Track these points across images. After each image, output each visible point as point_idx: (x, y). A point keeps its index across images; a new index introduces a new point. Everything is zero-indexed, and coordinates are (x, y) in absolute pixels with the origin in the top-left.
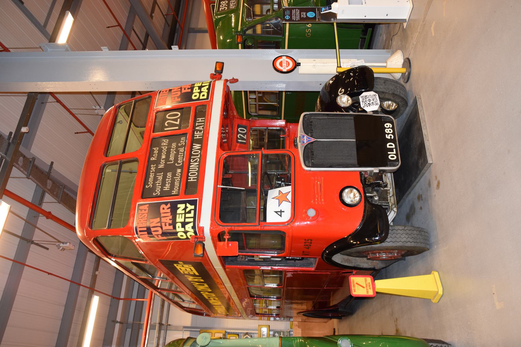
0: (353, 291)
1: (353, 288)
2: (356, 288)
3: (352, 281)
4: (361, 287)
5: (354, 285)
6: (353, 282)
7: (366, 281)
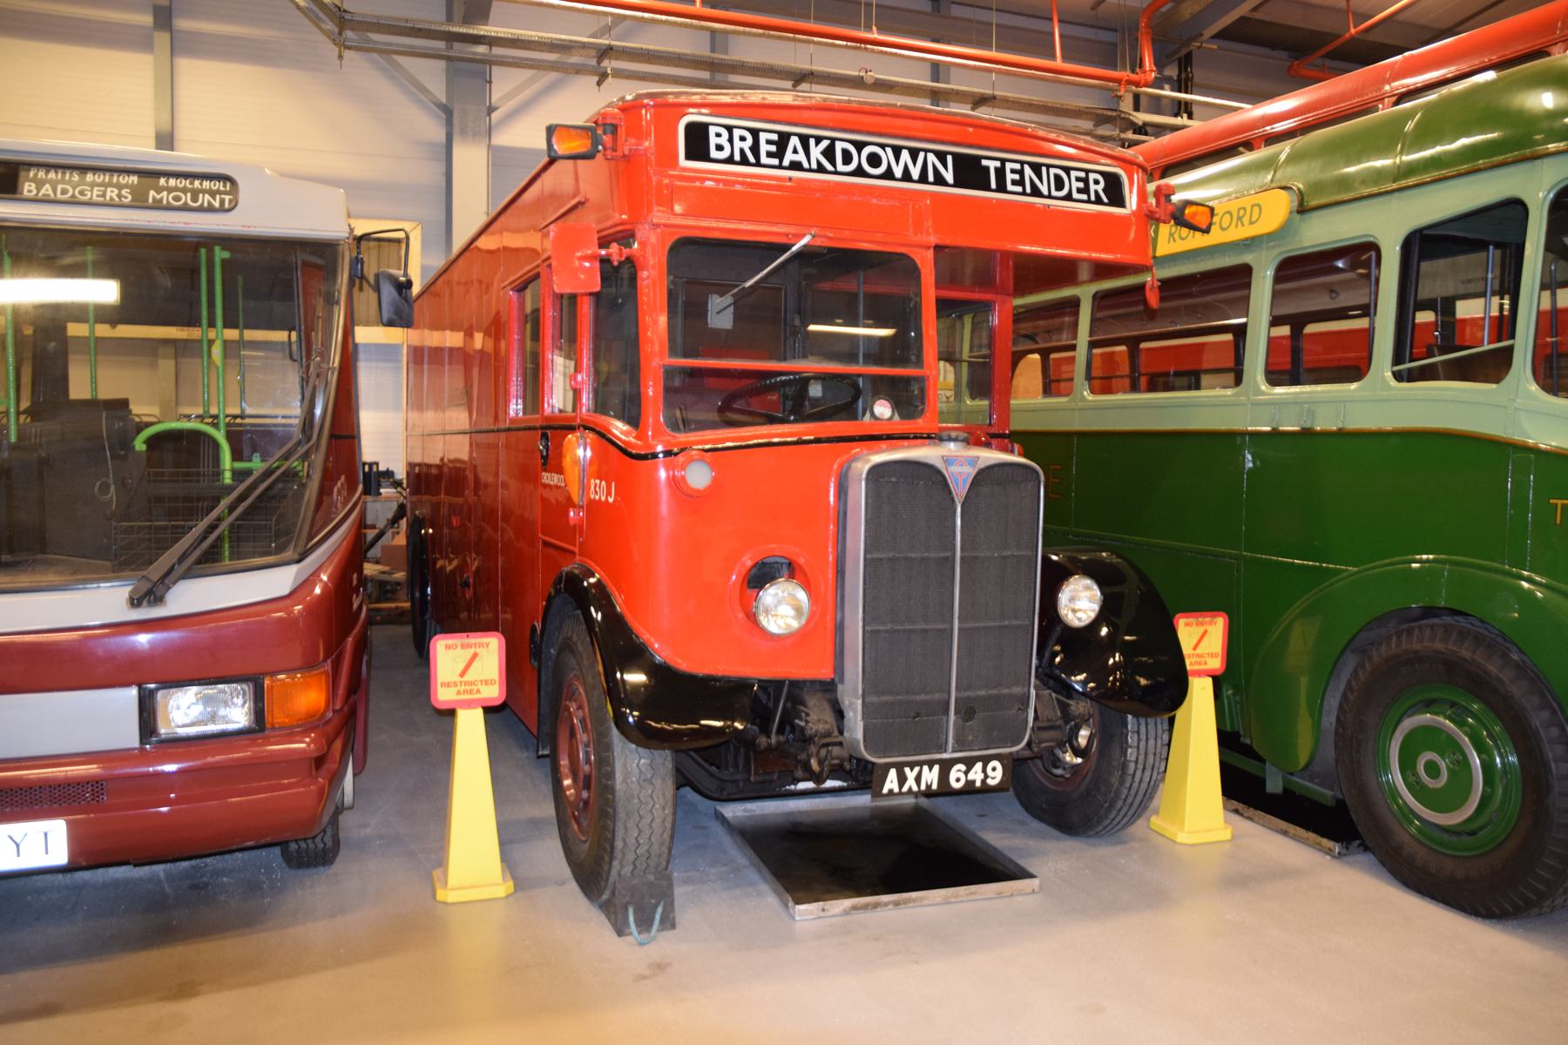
0: (450, 642)
1: (458, 642)
3: (486, 640)
5: (469, 646)
6: (481, 645)
7: (1212, 655)
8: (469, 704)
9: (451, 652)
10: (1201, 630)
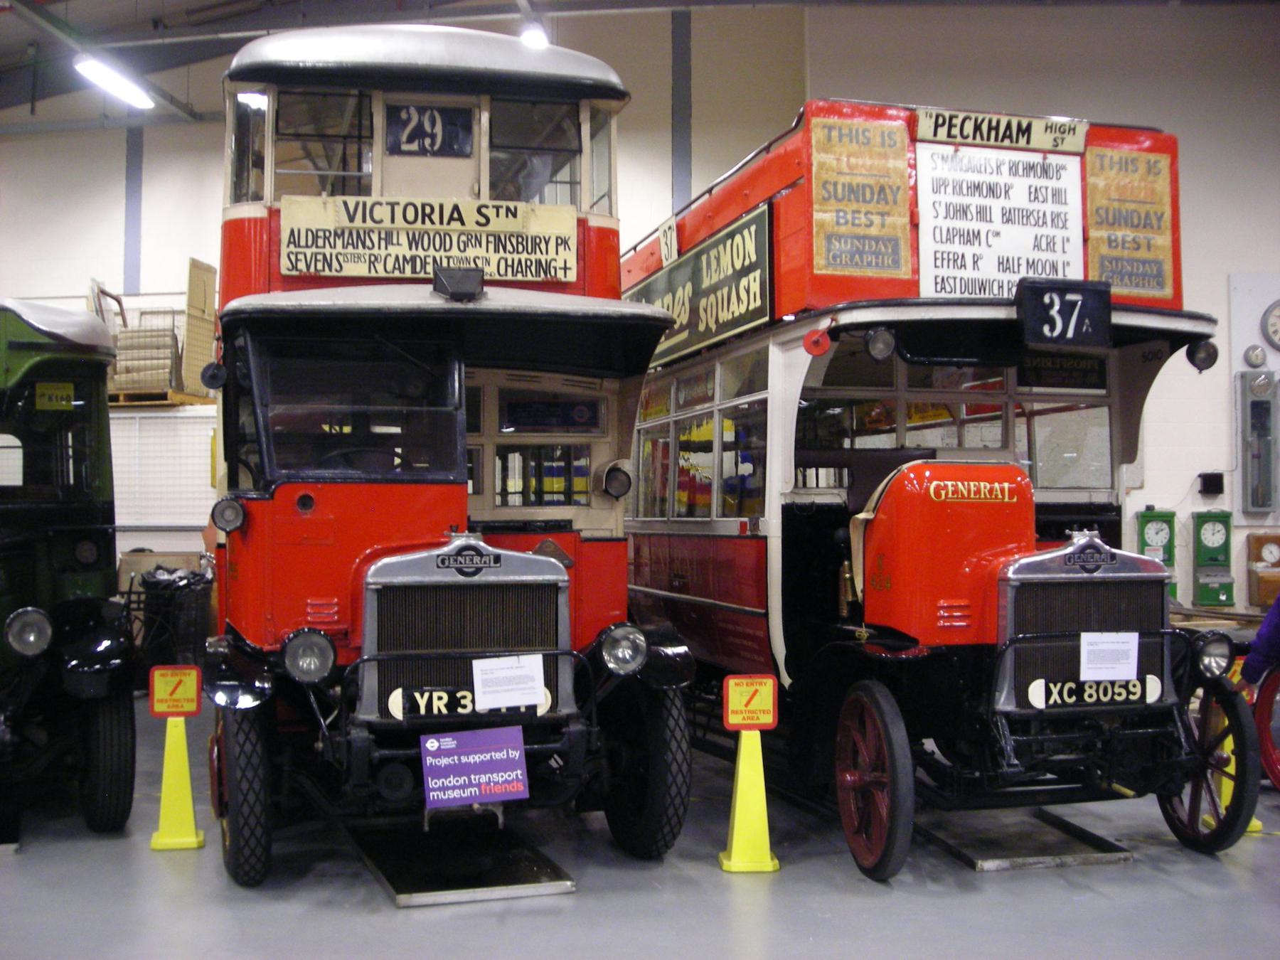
2: (744, 688)
4: (171, 689)
6: (761, 684)
7: (189, 700)
8: (750, 727)
9: (739, 689)
10: (177, 679)
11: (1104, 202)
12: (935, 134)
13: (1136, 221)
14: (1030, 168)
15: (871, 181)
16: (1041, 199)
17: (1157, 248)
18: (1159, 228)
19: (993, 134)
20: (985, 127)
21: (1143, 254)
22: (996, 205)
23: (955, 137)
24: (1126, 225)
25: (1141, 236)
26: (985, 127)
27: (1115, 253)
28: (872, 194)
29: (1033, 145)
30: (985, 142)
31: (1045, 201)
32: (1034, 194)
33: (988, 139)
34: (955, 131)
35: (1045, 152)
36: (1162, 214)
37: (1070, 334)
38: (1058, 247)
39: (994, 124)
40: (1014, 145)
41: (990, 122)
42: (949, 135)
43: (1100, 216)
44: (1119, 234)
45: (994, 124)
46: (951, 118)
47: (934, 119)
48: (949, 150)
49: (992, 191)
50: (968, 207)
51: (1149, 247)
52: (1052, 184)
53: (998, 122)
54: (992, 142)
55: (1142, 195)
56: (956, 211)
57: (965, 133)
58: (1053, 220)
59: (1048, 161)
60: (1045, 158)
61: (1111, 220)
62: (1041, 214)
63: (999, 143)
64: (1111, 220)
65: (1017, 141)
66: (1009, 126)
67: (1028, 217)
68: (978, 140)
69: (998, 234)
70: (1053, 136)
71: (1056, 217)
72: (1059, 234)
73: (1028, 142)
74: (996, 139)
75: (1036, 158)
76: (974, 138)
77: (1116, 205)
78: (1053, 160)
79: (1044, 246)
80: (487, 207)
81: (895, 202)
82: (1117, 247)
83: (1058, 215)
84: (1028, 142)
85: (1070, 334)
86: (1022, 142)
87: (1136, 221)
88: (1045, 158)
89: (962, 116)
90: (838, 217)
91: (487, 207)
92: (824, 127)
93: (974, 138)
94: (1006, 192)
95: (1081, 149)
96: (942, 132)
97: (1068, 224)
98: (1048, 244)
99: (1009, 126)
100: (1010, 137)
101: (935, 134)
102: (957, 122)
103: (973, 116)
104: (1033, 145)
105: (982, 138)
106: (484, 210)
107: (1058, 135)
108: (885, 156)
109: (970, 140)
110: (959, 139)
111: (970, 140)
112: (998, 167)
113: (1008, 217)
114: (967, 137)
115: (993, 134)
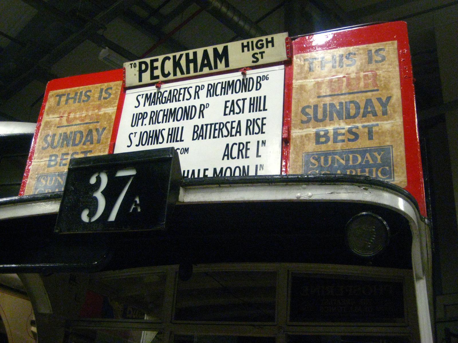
11: (313, 101)
12: (140, 80)
13: (353, 112)
14: (229, 86)
15: (82, 128)
16: (237, 110)
17: (383, 133)
18: (385, 113)
19: (192, 65)
20: (183, 62)
21: (363, 143)
22: (188, 126)
23: (158, 77)
24: (340, 117)
25: (360, 125)
26: (183, 62)
27: (323, 148)
28: (82, 137)
29: (232, 66)
30: (186, 75)
31: (242, 111)
32: (231, 108)
33: (188, 72)
34: (157, 72)
35: (243, 70)
36: (389, 98)
37: (113, 217)
38: (252, 153)
39: (191, 57)
40: (214, 71)
41: (187, 55)
42: (153, 77)
43: (306, 114)
44: (330, 128)
45: (191, 57)
46: (152, 62)
47: (137, 68)
48: (152, 90)
49: (187, 113)
50: (161, 132)
51: (370, 135)
52: (254, 94)
53: (195, 54)
54: (192, 73)
55: (362, 84)
56: (149, 137)
57: (166, 72)
58: (248, 127)
59: (248, 77)
60: (244, 74)
61: (320, 116)
62: (235, 125)
63: (199, 73)
64: (320, 116)
65: (216, 67)
66: (206, 54)
67: (221, 130)
68: (179, 75)
69: (186, 150)
70: (252, 52)
71: (251, 124)
72: (253, 139)
73: (227, 65)
74: (195, 70)
75: (238, 76)
76: (175, 74)
77: (328, 100)
78: (252, 74)
79: (235, 153)
80: (257, 54)
81: (99, 141)
82: (326, 142)
83: (255, 121)
84: (227, 65)
85: (113, 217)
86: (221, 66)
87: (353, 112)
88: (244, 74)
89: (161, 58)
90: (50, 161)
91: (257, 54)
92: (57, 96)
93: (175, 74)
94: (201, 112)
95: (284, 57)
96: (146, 77)
97: (265, 128)
98: (240, 150)
99: (206, 54)
100: (209, 65)
101: (140, 80)
102: (158, 64)
103: (171, 55)
104: (232, 66)
105: (182, 73)
106: (256, 56)
107: (256, 50)
108: (99, 107)
109: (171, 77)
110: (162, 78)
111: (171, 77)
112: (197, 92)
113: (199, 133)
114: (169, 74)
115: (192, 65)
